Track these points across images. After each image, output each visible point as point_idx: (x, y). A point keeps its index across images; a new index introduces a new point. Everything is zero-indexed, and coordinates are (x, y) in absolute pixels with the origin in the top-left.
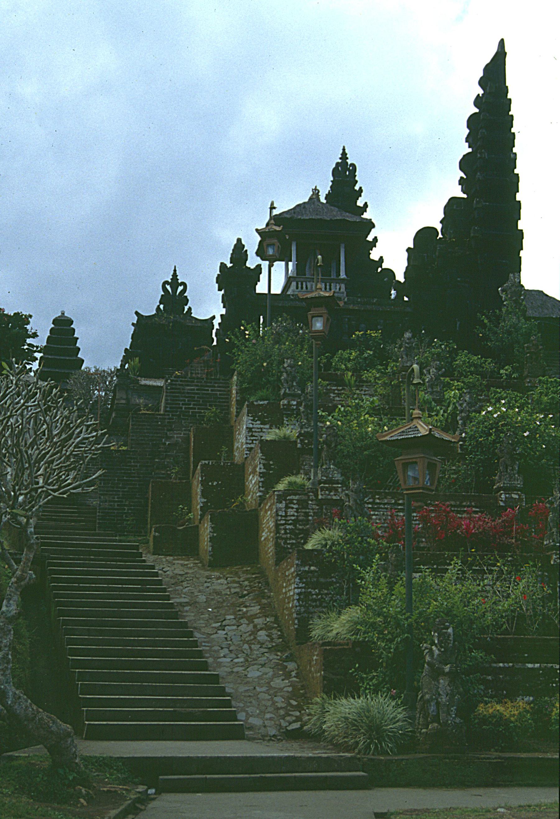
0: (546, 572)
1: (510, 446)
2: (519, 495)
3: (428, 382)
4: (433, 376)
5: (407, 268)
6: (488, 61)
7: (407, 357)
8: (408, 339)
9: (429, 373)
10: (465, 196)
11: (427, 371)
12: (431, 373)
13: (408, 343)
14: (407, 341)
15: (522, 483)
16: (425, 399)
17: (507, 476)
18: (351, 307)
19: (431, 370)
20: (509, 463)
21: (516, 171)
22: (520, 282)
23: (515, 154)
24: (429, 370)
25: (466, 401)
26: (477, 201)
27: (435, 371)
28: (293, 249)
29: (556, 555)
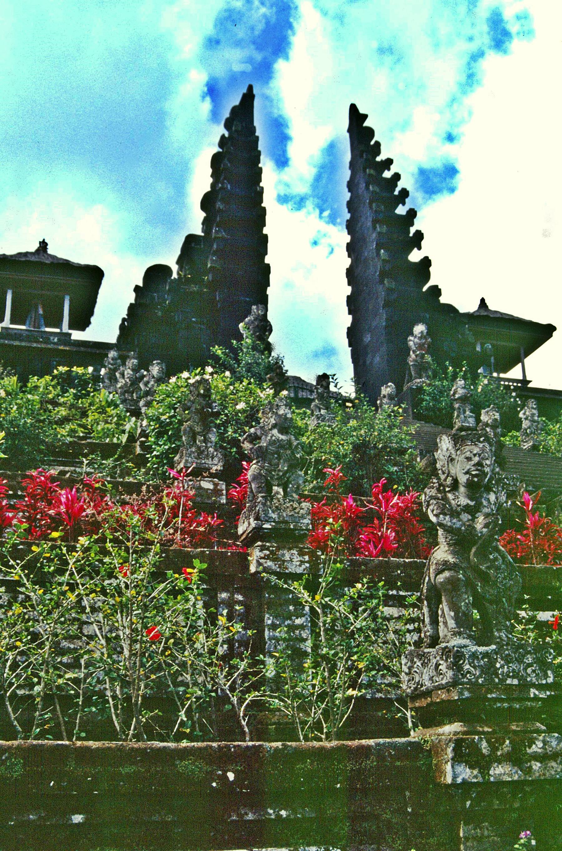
0: (239, 592)
1: (201, 400)
2: (216, 485)
3: (120, 388)
4: (128, 380)
5: (131, 308)
6: (271, 276)
7: (111, 381)
8: (113, 359)
9: (123, 377)
10: (203, 234)
11: (120, 373)
12: (126, 377)
13: (112, 364)
14: (112, 362)
15: (221, 464)
16: (109, 400)
17: (193, 449)
18: (61, 347)
19: (126, 373)
20: (198, 429)
21: (263, 205)
22: (265, 315)
23: (262, 188)
24: (124, 371)
25: (153, 377)
26: (216, 230)
27: (131, 373)
28: (8, 297)
29: (261, 551)
